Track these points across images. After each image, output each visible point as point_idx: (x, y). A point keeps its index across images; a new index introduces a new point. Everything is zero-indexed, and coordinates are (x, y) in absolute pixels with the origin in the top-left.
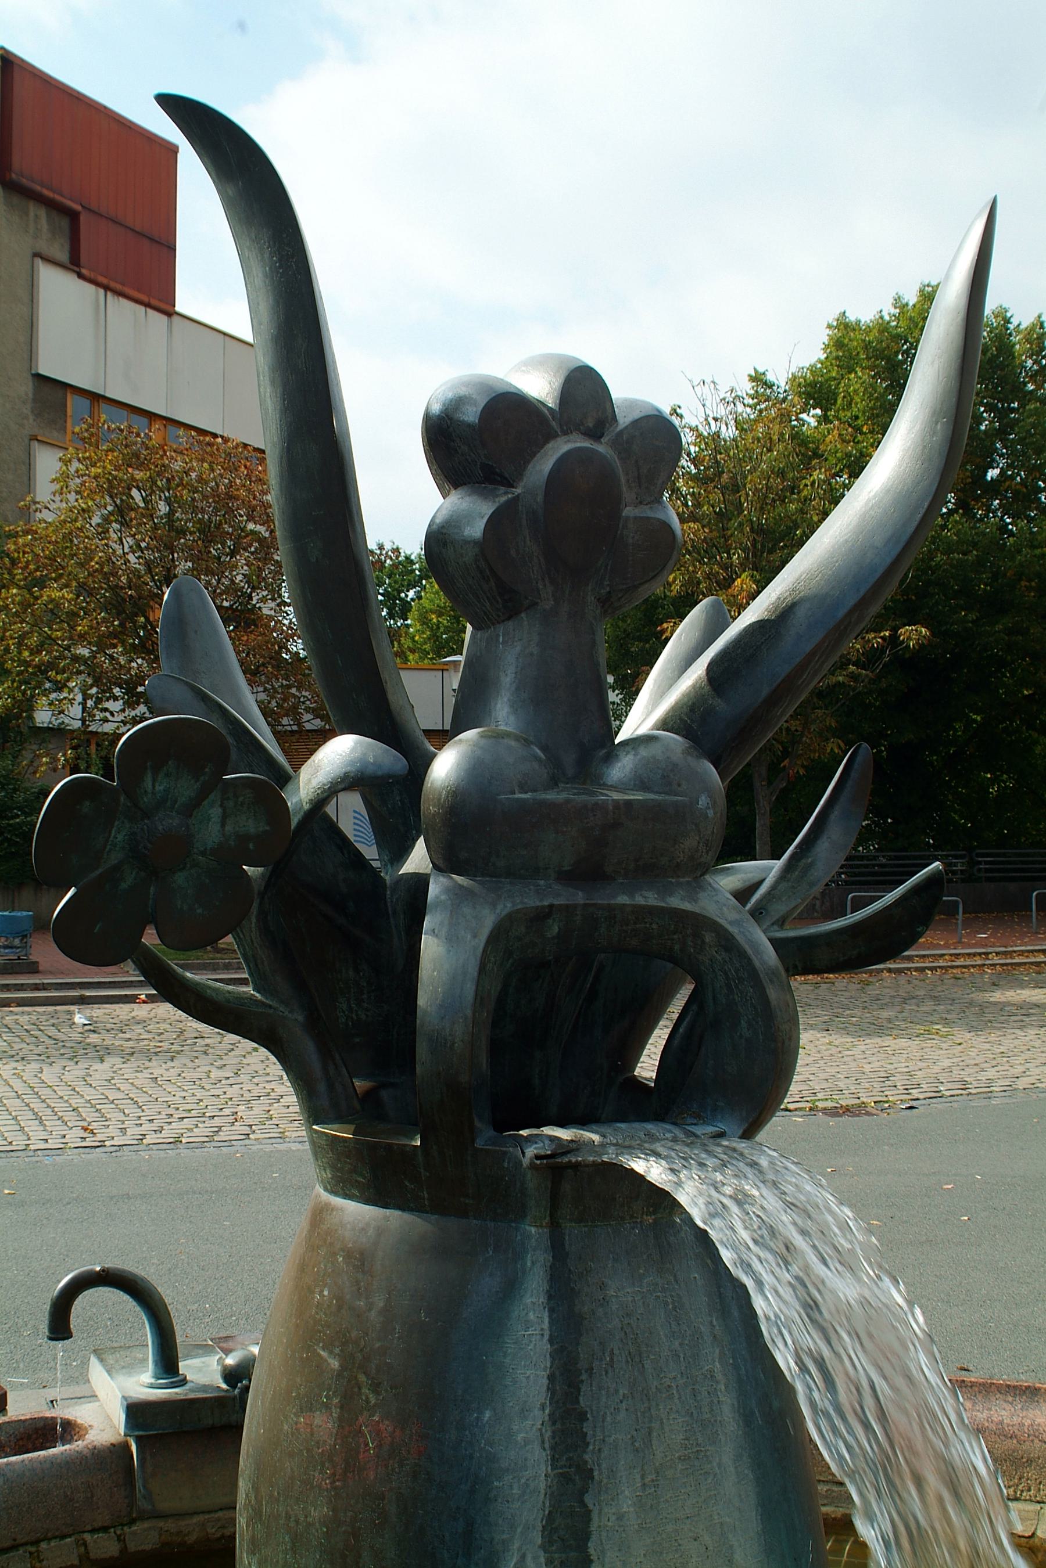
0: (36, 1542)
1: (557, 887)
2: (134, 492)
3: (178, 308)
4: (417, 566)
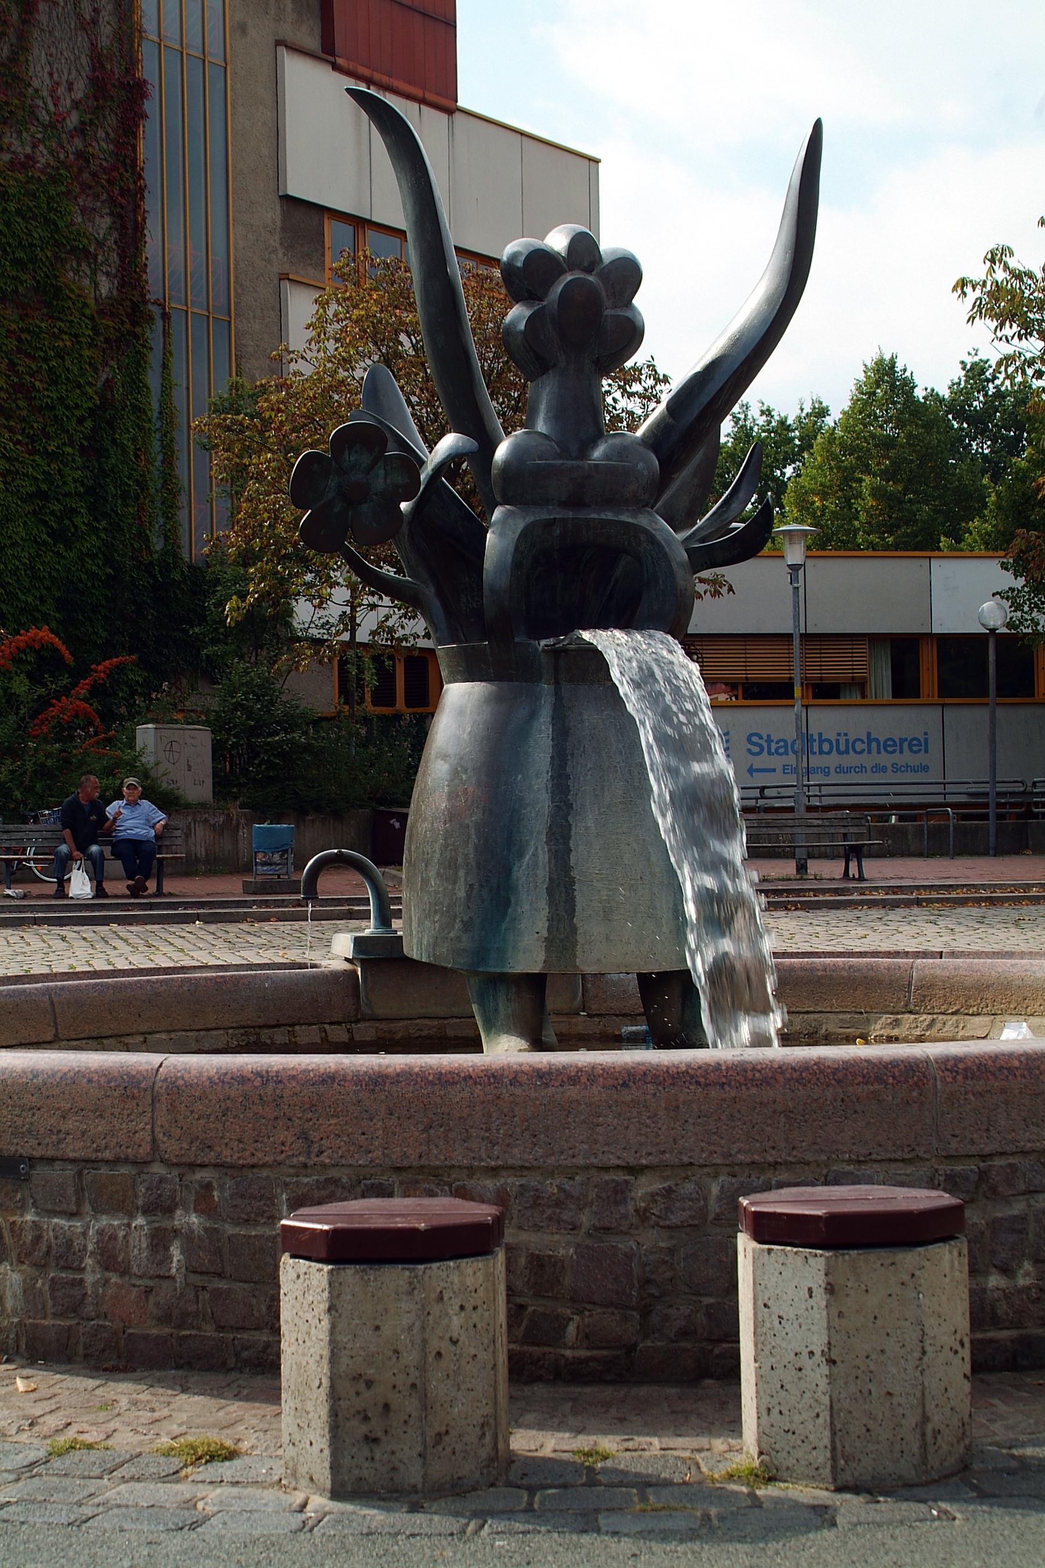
0: (292, 1025)
1: (558, 509)
2: (403, 337)
3: (459, 104)
4: (797, 433)
